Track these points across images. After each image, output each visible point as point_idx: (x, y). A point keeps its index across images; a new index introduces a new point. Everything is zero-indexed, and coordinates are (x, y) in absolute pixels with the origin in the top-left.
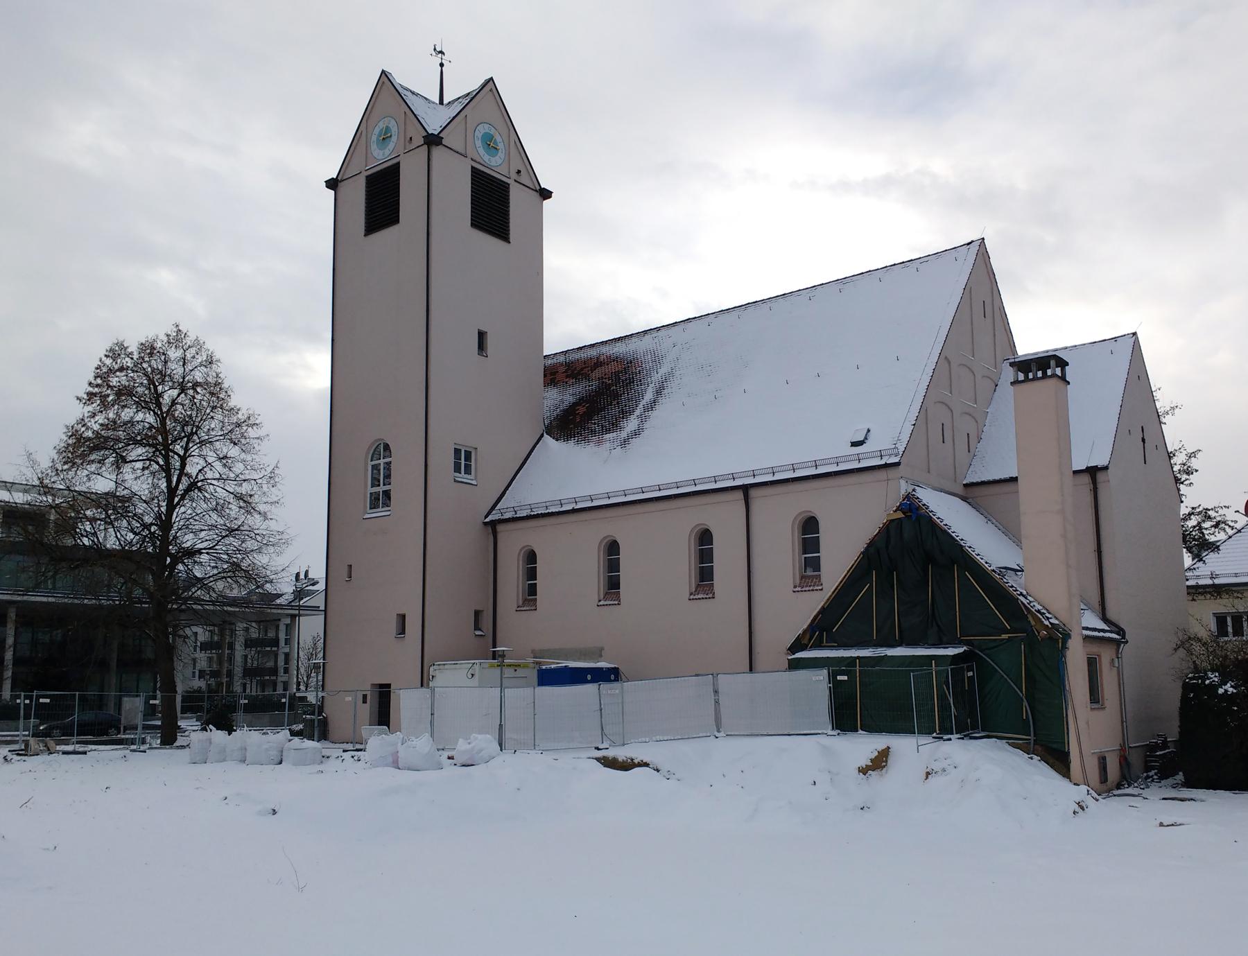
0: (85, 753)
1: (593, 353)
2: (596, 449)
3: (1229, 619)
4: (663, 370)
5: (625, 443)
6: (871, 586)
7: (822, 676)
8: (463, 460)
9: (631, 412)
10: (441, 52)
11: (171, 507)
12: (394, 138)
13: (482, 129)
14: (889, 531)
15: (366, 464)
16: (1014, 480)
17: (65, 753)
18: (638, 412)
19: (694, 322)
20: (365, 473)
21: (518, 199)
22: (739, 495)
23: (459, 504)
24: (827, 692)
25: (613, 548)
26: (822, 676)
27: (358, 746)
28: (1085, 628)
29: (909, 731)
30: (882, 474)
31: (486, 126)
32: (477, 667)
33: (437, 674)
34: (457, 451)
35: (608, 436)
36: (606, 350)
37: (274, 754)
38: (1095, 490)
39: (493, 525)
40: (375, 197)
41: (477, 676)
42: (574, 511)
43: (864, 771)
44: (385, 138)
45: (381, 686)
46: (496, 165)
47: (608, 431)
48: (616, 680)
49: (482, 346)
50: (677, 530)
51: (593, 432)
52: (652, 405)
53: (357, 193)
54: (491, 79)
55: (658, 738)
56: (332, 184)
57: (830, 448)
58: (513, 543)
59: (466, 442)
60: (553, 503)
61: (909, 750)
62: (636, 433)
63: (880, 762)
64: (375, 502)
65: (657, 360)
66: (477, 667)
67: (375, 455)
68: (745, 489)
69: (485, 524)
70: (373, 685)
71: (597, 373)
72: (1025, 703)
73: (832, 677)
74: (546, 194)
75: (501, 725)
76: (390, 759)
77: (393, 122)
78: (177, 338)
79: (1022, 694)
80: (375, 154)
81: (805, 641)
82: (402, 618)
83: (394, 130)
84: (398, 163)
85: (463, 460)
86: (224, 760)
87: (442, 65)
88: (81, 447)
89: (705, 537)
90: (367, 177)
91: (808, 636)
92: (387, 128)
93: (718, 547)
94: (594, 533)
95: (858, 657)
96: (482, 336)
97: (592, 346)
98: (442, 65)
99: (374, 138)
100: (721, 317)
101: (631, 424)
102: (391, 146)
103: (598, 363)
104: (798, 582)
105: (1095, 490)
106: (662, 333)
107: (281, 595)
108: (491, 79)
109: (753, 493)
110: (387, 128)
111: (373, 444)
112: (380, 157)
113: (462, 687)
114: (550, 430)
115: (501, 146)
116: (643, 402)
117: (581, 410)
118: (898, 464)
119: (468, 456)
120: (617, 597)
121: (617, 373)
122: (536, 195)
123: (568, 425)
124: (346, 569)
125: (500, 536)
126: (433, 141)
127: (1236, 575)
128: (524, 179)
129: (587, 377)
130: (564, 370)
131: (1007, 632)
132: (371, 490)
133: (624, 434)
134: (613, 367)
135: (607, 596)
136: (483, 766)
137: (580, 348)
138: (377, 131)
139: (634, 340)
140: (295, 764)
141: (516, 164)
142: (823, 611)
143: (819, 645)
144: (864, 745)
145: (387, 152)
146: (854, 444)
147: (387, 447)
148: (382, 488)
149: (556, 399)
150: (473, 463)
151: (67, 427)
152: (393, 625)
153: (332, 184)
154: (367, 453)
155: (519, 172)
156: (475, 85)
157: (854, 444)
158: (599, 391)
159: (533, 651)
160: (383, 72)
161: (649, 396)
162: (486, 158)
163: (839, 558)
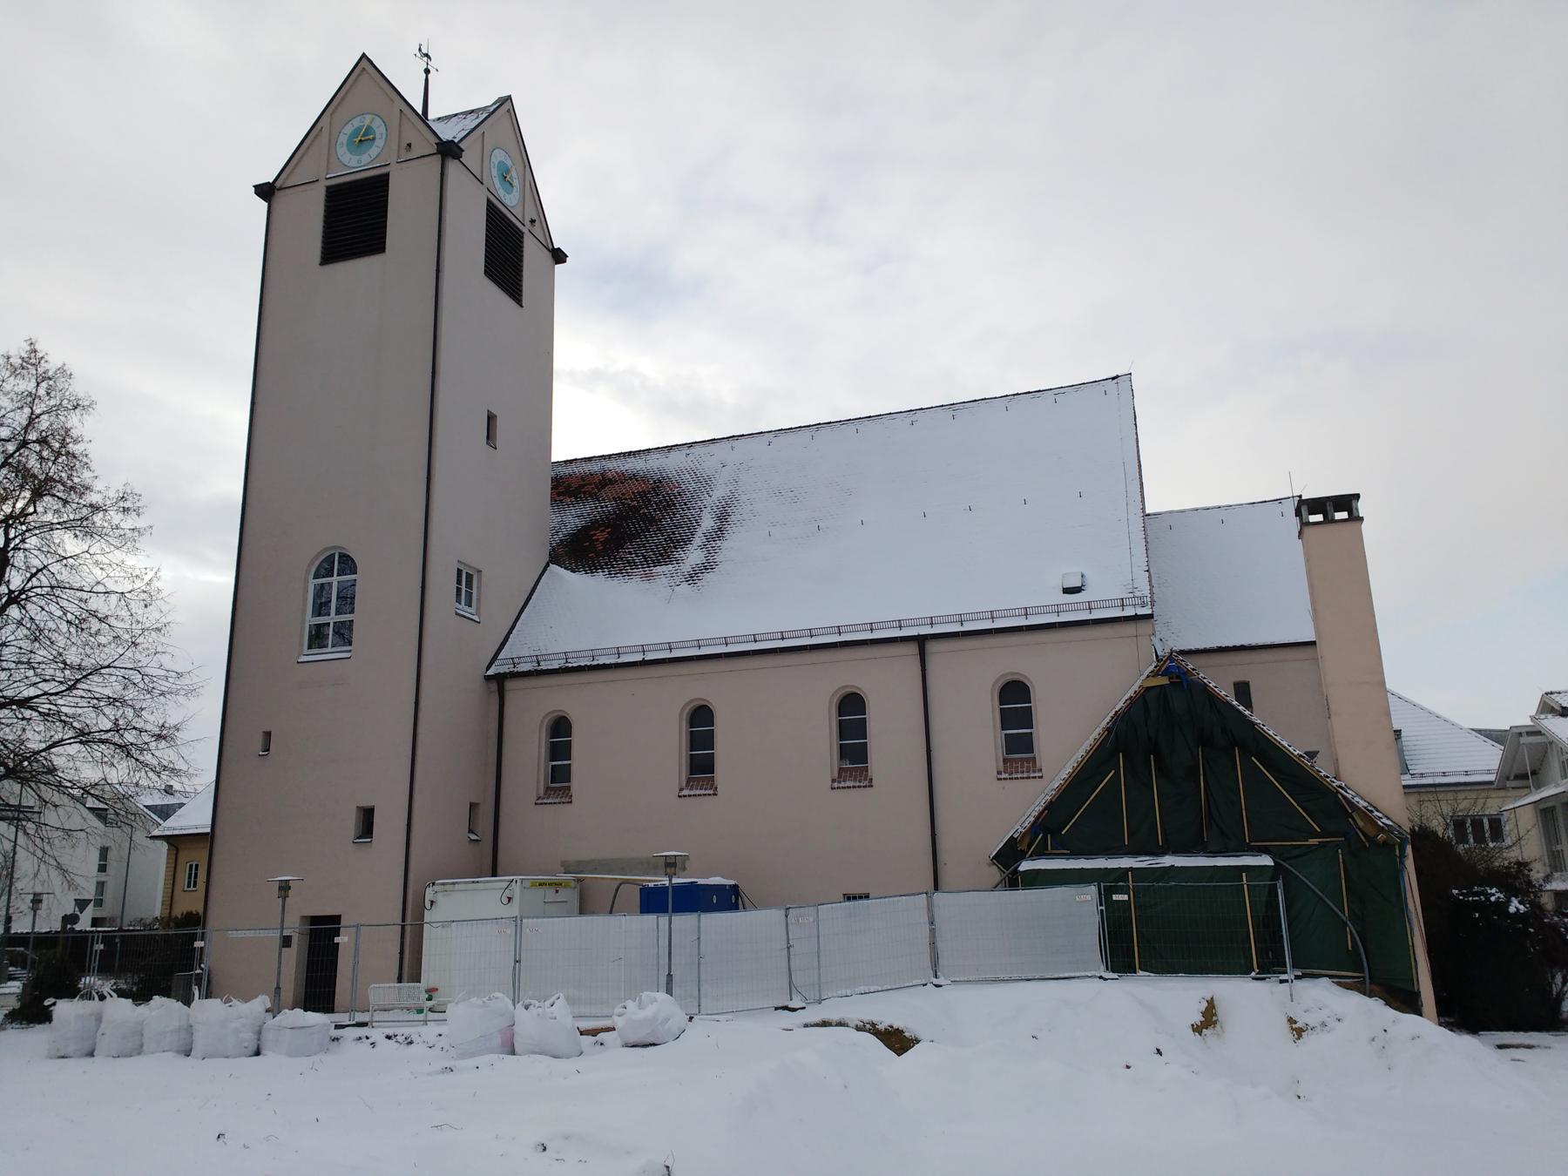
1: (595, 468)
3: (1486, 821)
4: (719, 493)
5: (692, 578)
6: (1117, 774)
7: (1090, 893)
8: (466, 581)
9: (688, 541)
10: (427, 55)
12: (380, 142)
14: (1142, 701)
15: (307, 581)
16: (1313, 643)
19: (743, 440)
20: (305, 590)
22: (913, 649)
23: (459, 651)
24: (1097, 918)
25: (701, 716)
26: (1090, 893)
27: (360, 1017)
29: (1245, 970)
30: (1130, 629)
32: (516, 888)
33: (440, 899)
34: (459, 572)
35: (659, 569)
36: (610, 465)
37: (248, 1037)
39: (500, 679)
43: (1198, 1029)
44: (363, 140)
45: (315, 920)
46: (511, 200)
47: (657, 563)
49: (490, 436)
51: (632, 564)
52: (719, 533)
53: (310, 212)
54: (509, 98)
55: (863, 989)
56: (265, 191)
57: (1030, 591)
58: (530, 712)
59: (475, 560)
61: (1248, 999)
63: (1209, 1019)
64: (317, 638)
65: (706, 482)
66: (516, 888)
67: (325, 569)
68: (921, 641)
69: (488, 678)
70: (303, 918)
71: (607, 492)
72: (1350, 927)
73: (1105, 896)
74: (559, 256)
76: (497, 1041)
77: (378, 121)
79: (1345, 916)
81: (1023, 847)
83: (379, 129)
85: (466, 581)
87: (427, 71)
89: (851, 706)
91: (1027, 841)
92: (369, 130)
95: (1131, 869)
96: (491, 418)
98: (427, 71)
99: (343, 139)
100: (782, 436)
101: (693, 556)
102: (374, 151)
103: (623, 478)
104: (542, 793)
108: (509, 98)
109: (932, 647)
110: (369, 130)
111: (326, 549)
112: (353, 164)
113: (470, 921)
114: (555, 558)
115: (516, 183)
117: (601, 536)
118: (1150, 616)
119: (470, 577)
120: (711, 785)
121: (643, 494)
122: (548, 255)
123: (582, 551)
125: (509, 697)
126: (449, 151)
127: (1467, 773)
129: (595, 497)
130: (573, 484)
131: (1317, 835)
134: (634, 487)
135: (690, 783)
136: (672, 1043)
141: (530, 213)
142: (1050, 806)
143: (1041, 853)
144: (1182, 995)
146: (1067, 591)
148: (332, 618)
149: (573, 518)
150: (474, 591)
152: (351, 822)
153: (265, 191)
156: (487, 100)
157: (1067, 591)
158: (625, 517)
159: (563, 864)
161: (707, 522)
162: (501, 193)
163: (1067, 736)
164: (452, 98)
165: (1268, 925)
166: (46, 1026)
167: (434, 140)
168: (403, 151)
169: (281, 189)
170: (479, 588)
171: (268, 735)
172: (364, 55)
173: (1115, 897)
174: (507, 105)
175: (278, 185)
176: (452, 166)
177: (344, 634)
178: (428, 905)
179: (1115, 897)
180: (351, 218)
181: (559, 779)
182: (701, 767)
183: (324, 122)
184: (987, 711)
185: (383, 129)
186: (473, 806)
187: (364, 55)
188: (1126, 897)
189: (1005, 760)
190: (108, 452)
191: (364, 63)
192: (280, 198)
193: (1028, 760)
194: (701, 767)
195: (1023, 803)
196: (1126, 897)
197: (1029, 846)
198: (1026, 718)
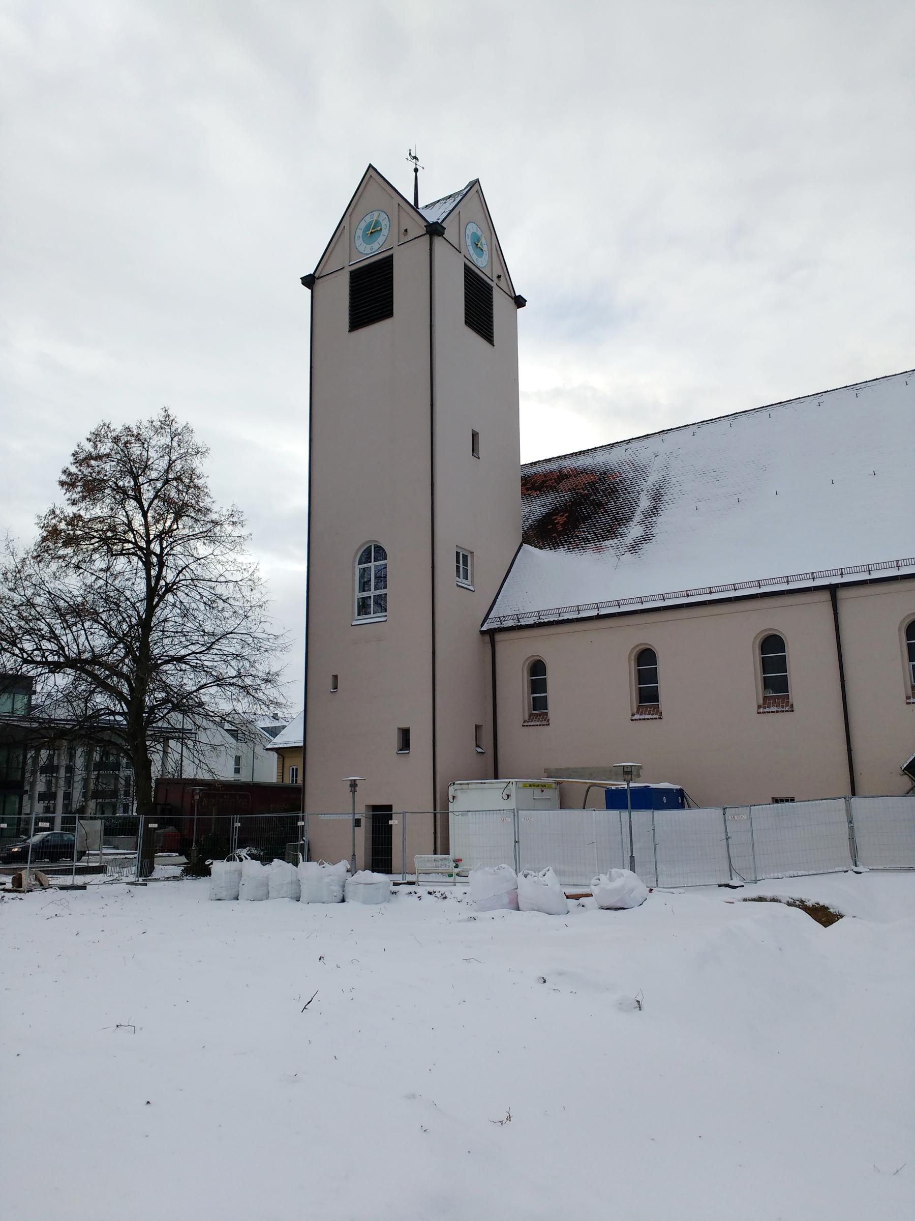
0: (83, 887)
1: (554, 466)
2: (597, 556)
8: (463, 560)
10: (415, 158)
11: (151, 610)
12: (385, 232)
13: (472, 228)
17: (63, 888)
18: (637, 517)
20: (354, 575)
21: (500, 302)
22: (826, 596)
23: (461, 613)
27: (410, 878)
31: (475, 226)
32: (513, 788)
33: (459, 794)
39: (491, 634)
40: (365, 292)
41: (513, 796)
42: (599, 617)
44: (373, 231)
45: (375, 808)
46: (481, 263)
48: (681, 806)
50: (616, 650)
52: (654, 511)
53: (339, 291)
56: (309, 281)
58: (514, 657)
60: (568, 609)
62: (646, 538)
64: (363, 607)
67: (366, 557)
68: (833, 589)
69: (483, 633)
74: (520, 302)
76: (506, 900)
80: (361, 249)
82: (405, 734)
83: (384, 222)
84: (392, 256)
85: (463, 560)
86: (267, 896)
87: (416, 170)
88: (59, 536)
90: (351, 272)
92: (377, 222)
93: (794, 655)
94: (624, 642)
96: (475, 435)
97: (549, 460)
98: (416, 170)
99: (359, 233)
100: (705, 427)
101: (634, 531)
102: (381, 239)
104: (761, 702)
106: (634, 445)
107: (286, 706)
109: (842, 594)
110: (377, 222)
112: (367, 251)
113: (480, 810)
114: (527, 539)
115: (485, 248)
116: (638, 511)
117: (561, 519)
119: (465, 557)
120: (657, 710)
123: (546, 533)
126: (435, 230)
128: (502, 283)
129: (554, 489)
130: (537, 481)
132: (359, 595)
133: (629, 540)
134: (583, 479)
137: (535, 463)
138: (363, 225)
139: (599, 453)
140: (365, 903)
141: (497, 271)
145: (376, 246)
148: (373, 593)
150: (469, 568)
151: (39, 517)
152: (394, 739)
153: (309, 281)
155: (499, 277)
156: (461, 185)
158: (579, 504)
159: (546, 770)
160: (370, 166)
161: (645, 503)
162: (474, 258)
164: (435, 189)
166: (203, 879)
168: (402, 236)
169: (319, 278)
171: (336, 677)
174: (476, 187)
175: (316, 275)
176: (438, 241)
177: (381, 603)
178: (451, 799)
182: (648, 697)
190: (221, 483)
192: (319, 285)
194: (648, 697)
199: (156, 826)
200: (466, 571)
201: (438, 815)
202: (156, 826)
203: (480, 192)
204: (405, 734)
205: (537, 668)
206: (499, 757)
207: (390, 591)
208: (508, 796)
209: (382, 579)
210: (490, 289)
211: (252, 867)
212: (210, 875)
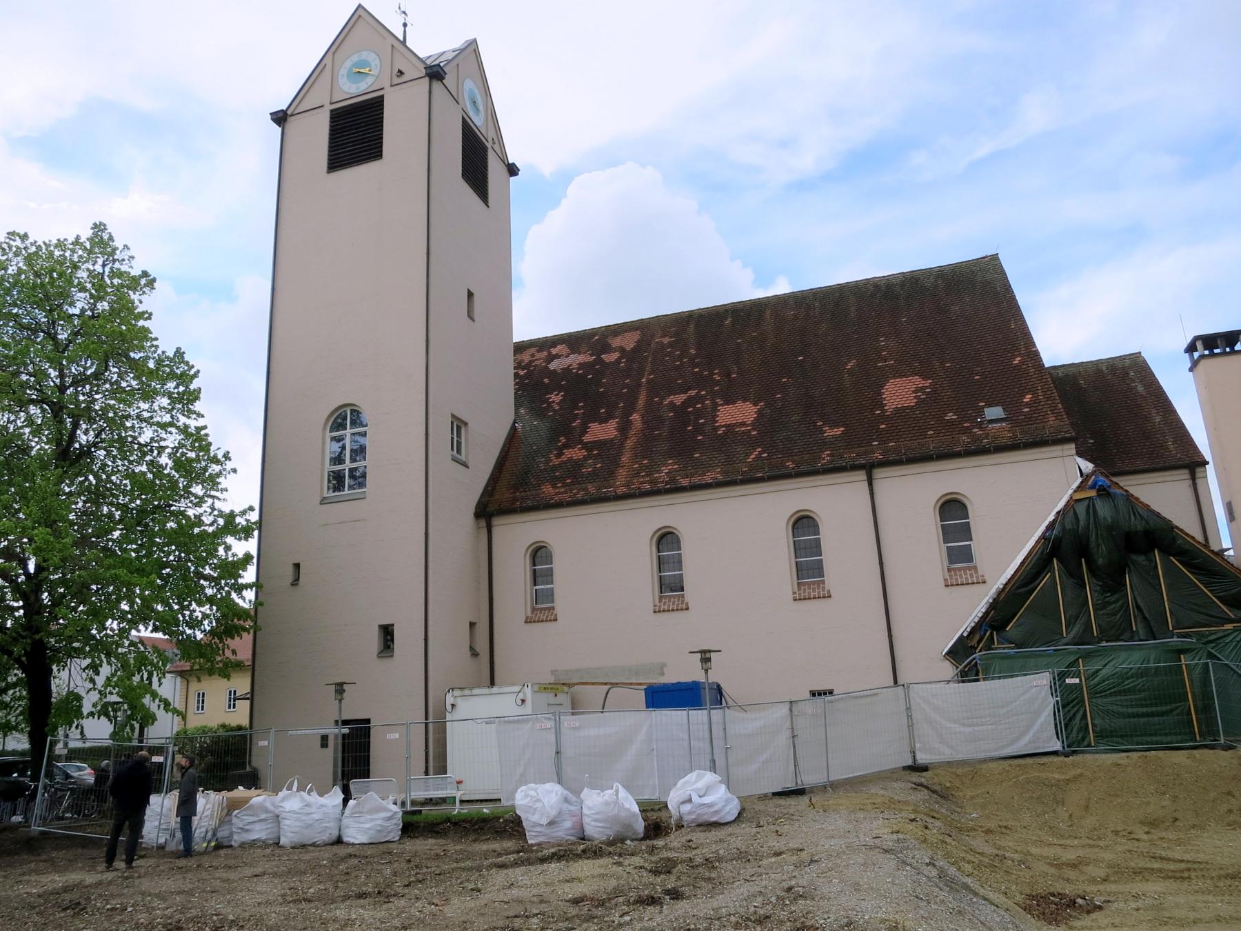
21: (495, 169)
28: (427, 773)
32: (528, 692)
33: (459, 702)
38: (1195, 485)
41: (529, 702)
46: (478, 121)
53: (315, 134)
54: (475, 40)
56: (280, 118)
67: (339, 424)
74: (513, 170)
75: (908, 709)
78: (100, 242)
81: (974, 642)
82: (387, 633)
85: (458, 425)
87: (405, 25)
91: (977, 637)
93: (828, 537)
96: (470, 295)
98: (405, 25)
99: (343, 72)
104: (529, 614)
105: (1195, 485)
112: (351, 90)
124: (290, 571)
125: (495, 531)
126: (435, 73)
128: (497, 147)
131: (1231, 621)
147: (356, 413)
148: (347, 465)
152: (373, 640)
153: (280, 118)
154: (324, 428)
156: (458, 43)
162: (471, 114)
164: (429, 43)
165: (1206, 709)
166: (389, 660)
167: (422, 67)
168: (395, 78)
169: (292, 115)
170: (466, 439)
171: (297, 566)
172: (360, 6)
173: (1068, 681)
174: (473, 47)
175: (289, 112)
176: (437, 85)
177: (359, 479)
178: (449, 708)
179: (1068, 681)
180: (355, 133)
181: (542, 607)
182: (671, 586)
183: (328, 61)
184: (930, 525)
185: (377, 62)
186: (472, 625)
187: (360, 6)
188: (1077, 681)
189: (949, 570)
190: (169, 324)
191: (360, 12)
192: (292, 123)
193: (970, 568)
194: (671, 586)
195: (972, 606)
196: (1077, 681)
197: (979, 642)
198: (965, 532)
199: (31, 567)
200: (459, 443)
201: (431, 727)
202: (31, 567)
203: (476, 52)
204: (387, 633)
205: (539, 553)
206: (868, 496)
207: (370, 463)
208: (523, 701)
209: (359, 452)
210: (485, 149)
211: (80, 850)
212: (995, 258)
